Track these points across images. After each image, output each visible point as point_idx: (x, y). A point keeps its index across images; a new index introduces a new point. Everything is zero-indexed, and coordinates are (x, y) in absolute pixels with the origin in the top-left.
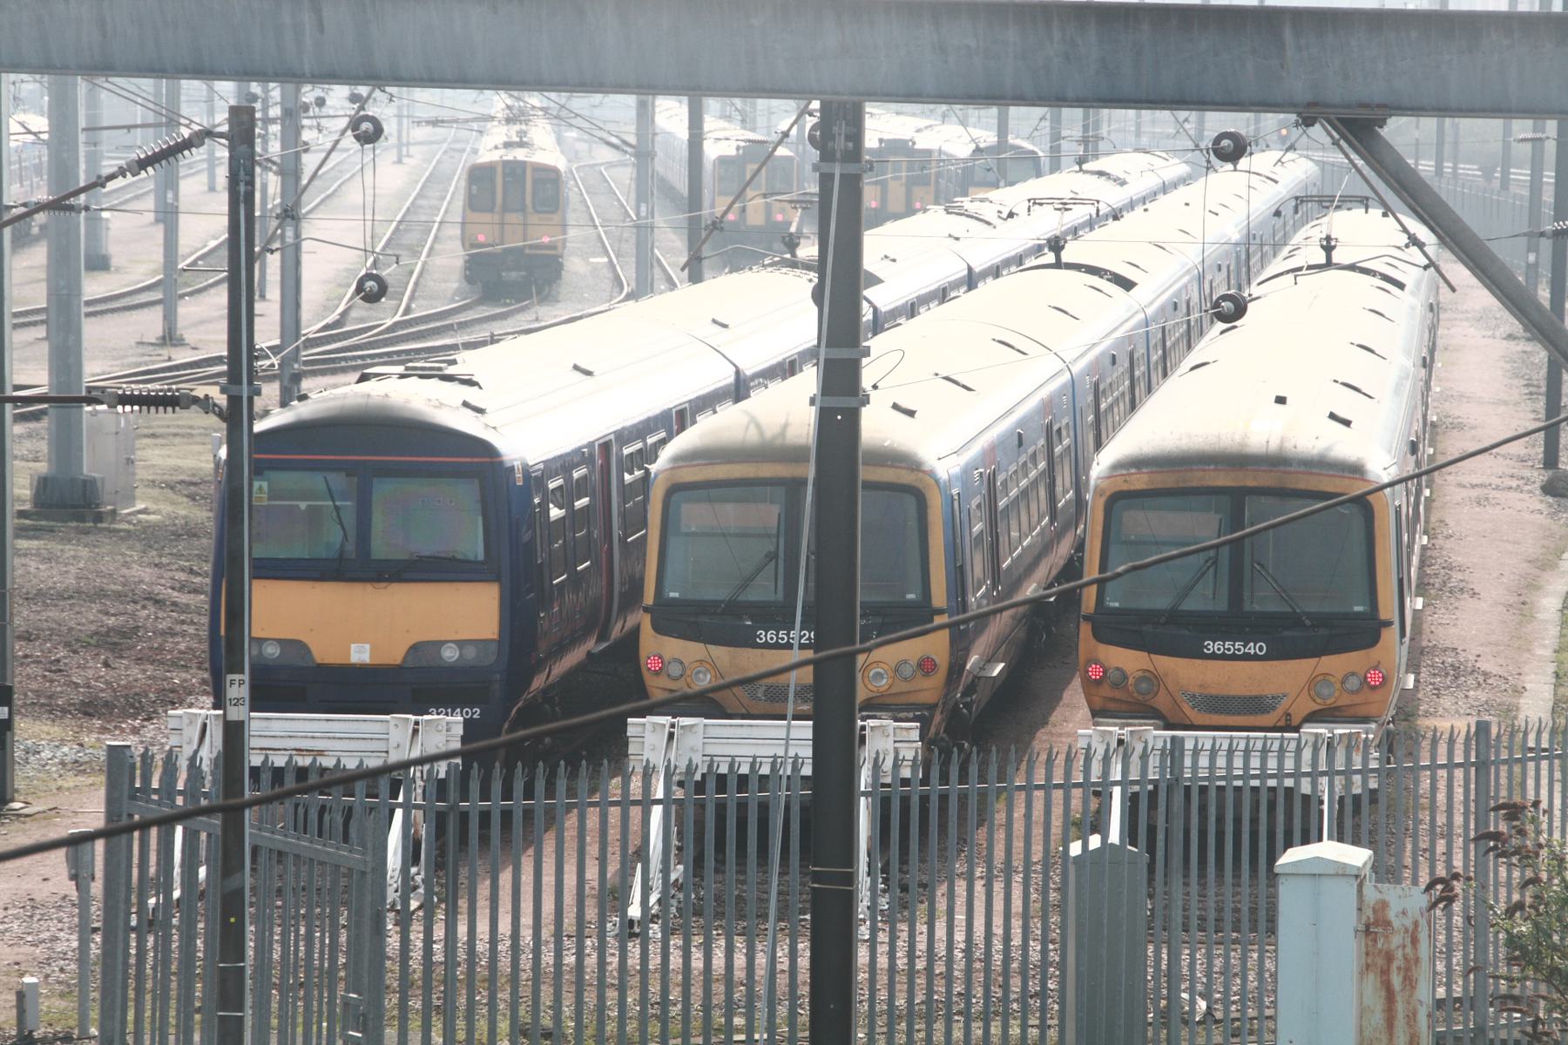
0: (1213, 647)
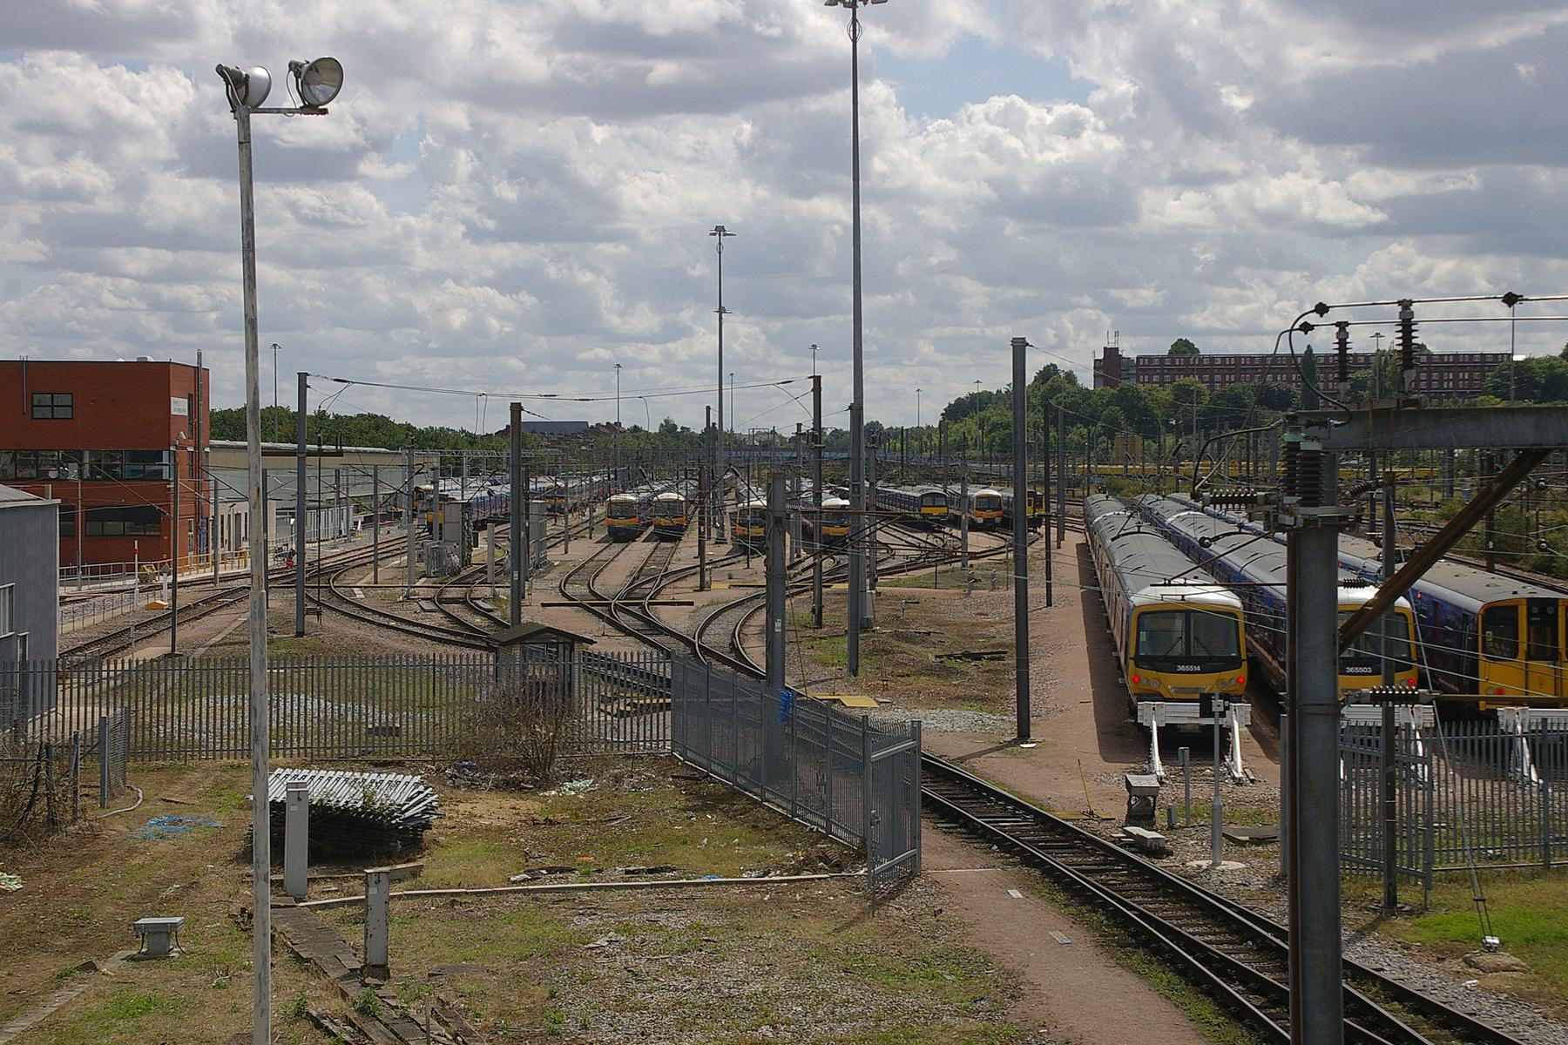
0: (1181, 668)
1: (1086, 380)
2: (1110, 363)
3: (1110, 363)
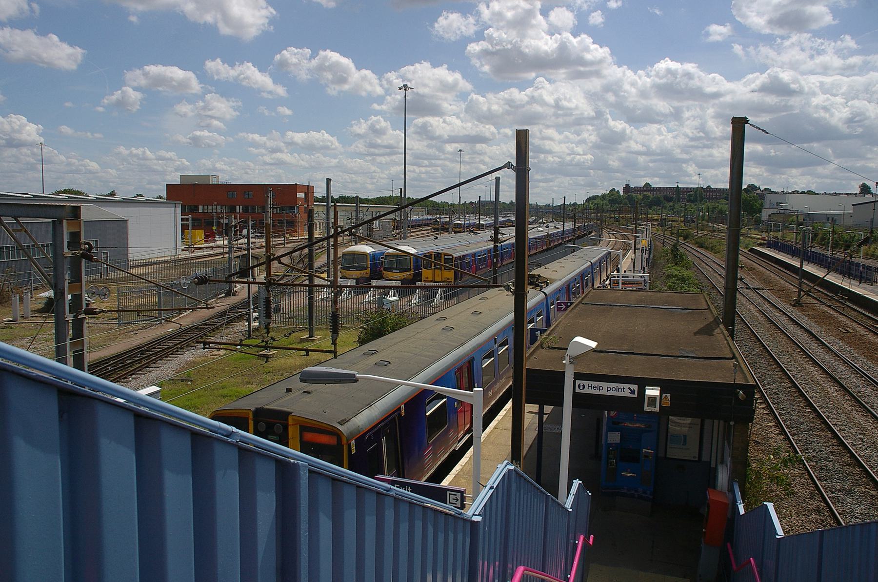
1: (621, 193)
2: (627, 188)
3: (627, 188)
